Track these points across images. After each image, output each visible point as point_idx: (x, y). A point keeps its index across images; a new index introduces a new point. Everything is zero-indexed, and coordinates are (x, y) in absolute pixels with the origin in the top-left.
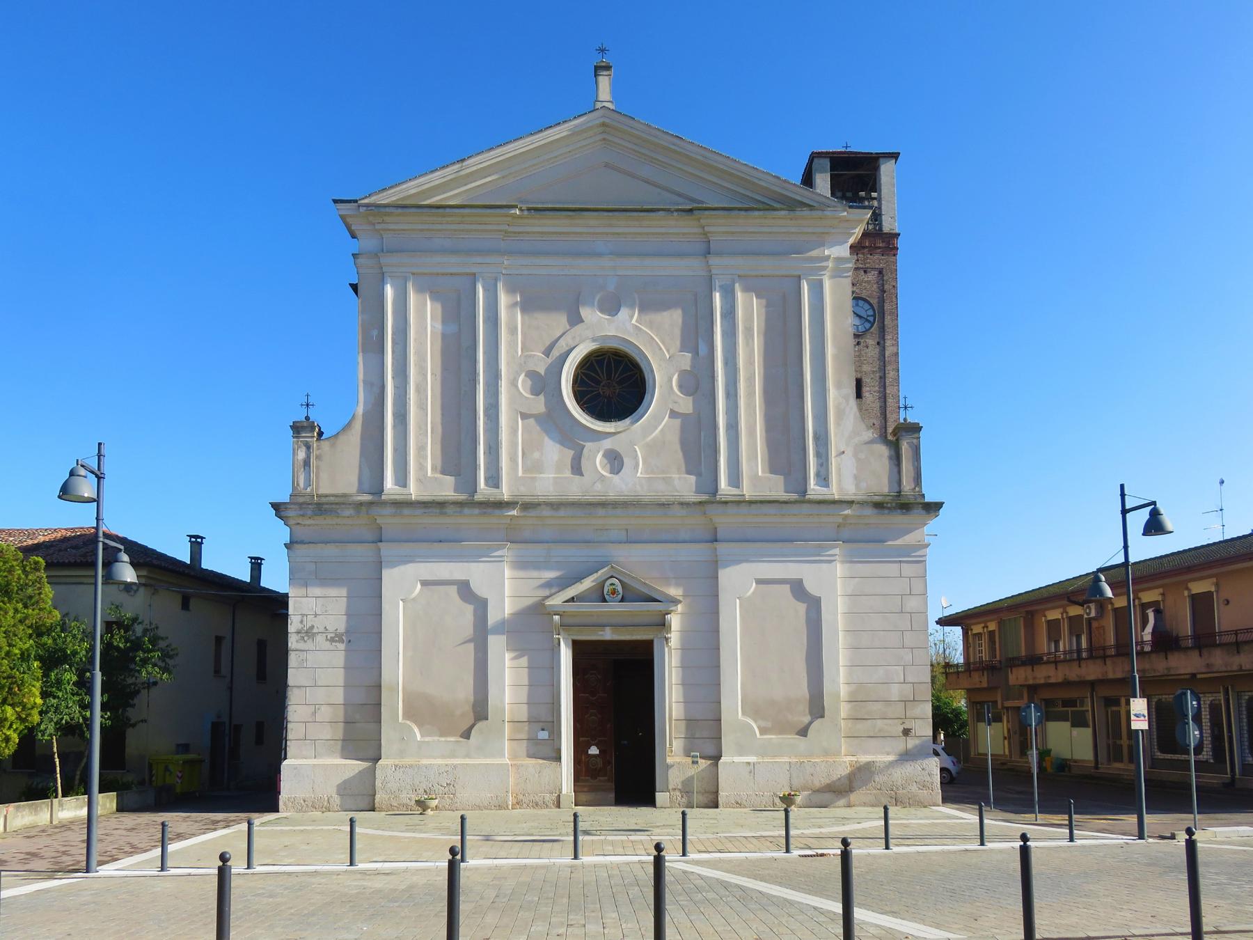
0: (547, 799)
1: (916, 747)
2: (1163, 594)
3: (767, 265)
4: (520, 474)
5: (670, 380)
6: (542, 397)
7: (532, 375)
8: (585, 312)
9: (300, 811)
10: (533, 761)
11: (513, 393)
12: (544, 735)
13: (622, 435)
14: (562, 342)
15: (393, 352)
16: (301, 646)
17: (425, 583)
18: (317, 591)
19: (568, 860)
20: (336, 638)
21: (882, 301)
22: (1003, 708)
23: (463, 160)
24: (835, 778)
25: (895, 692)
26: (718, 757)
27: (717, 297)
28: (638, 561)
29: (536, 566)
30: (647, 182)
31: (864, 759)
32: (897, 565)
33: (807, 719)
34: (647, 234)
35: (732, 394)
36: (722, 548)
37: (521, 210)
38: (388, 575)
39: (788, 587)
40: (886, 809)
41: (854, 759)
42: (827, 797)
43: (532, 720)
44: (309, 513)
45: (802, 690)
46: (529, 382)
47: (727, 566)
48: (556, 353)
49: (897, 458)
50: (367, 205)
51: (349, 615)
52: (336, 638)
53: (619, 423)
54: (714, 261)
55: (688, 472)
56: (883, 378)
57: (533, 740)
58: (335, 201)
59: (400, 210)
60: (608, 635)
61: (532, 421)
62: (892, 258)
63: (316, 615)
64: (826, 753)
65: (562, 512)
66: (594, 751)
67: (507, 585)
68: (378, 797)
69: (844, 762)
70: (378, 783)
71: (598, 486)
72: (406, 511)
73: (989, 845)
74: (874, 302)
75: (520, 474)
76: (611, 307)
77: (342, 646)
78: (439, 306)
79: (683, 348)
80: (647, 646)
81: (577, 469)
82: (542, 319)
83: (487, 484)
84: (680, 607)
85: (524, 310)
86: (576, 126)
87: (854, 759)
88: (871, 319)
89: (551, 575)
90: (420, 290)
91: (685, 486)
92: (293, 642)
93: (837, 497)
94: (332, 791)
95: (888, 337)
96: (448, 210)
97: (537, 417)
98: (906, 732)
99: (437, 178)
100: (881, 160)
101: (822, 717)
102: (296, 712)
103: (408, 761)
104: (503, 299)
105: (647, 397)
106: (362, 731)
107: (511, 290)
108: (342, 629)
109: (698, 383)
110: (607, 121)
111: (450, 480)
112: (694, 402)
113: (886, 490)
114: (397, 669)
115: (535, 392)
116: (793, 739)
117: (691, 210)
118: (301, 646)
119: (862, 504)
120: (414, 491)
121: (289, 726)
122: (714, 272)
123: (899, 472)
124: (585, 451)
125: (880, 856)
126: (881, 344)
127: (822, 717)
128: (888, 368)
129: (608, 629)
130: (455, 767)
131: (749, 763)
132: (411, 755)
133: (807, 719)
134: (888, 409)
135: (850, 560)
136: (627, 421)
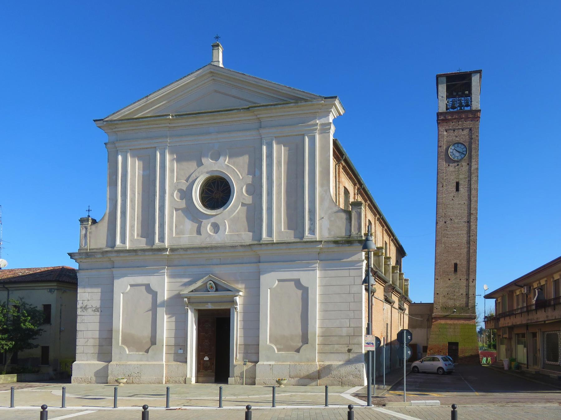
0: (180, 380)
1: (354, 358)
2: (546, 281)
4: (174, 236)
5: (242, 189)
6: (184, 201)
7: (180, 191)
8: (204, 160)
9: (80, 383)
10: (176, 363)
11: (171, 199)
12: (181, 351)
13: (219, 216)
14: (194, 175)
15: (121, 185)
16: (82, 313)
17: (132, 286)
18: (89, 290)
19: (111, 408)
20: (96, 310)
21: (470, 143)
23: (147, 96)
24: (311, 372)
25: (344, 332)
26: (257, 362)
27: (264, 148)
28: (223, 273)
29: (180, 276)
30: (234, 97)
31: (327, 363)
33: (300, 344)
34: (232, 121)
35: (270, 194)
36: (262, 265)
37: (172, 116)
38: (117, 282)
39: (293, 283)
40: (326, 387)
41: (323, 363)
42: (307, 380)
43: (176, 345)
44: (84, 257)
45: (299, 331)
46: (179, 194)
47: (265, 274)
48: (191, 180)
49: (349, 219)
50: (107, 121)
51: (102, 300)
52: (96, 310)
53: (218, 210)
54: (262, 131)
55: (249, 231)
56: (470, 181)
57: (176, 354)
58: (95, 121)
59: (120, 122)
60: (210, 307)
61: (180, 211)
63: (88, 300)
64: (308, 360)
65: (189, 252)
66: (206, 358)
67: (166, 286)
68: (109, 377)
69: (318, 364)
70: (109, 372)
71: (208, 240)
72: (122, 254)
73: (278, 407)
74: (467, 144)
75: (174, 236)
76: (216, 158)
77: (98, 313)
78: (141, 163)
79: (249, 174)
80: (229, 310)
81: (199, 232)
82: (185, 164)
83: (159, 240)
84: (241, 293)
85: (177, 162)
86: (198, 75)
87: (323, 363)
89: (186, 280)
90: (133, 156)
91: (247, 237)
92: (79, 312)
93: (318, 239)
94: (92, 375)
95: (473, 161)
96: (140, 120)
97: (183, 210)
98: (349, 351)
99: (137, 106)
101: (307, 343)
102: (80, 341)
103: (123, 362)
104: (168, 157)
105: (231, 197)
106: (105, 351)
107: (171, 153)
108: (98, 306)
109: (254, 189)
110: (212, 70)
111: (144, 240)
112: (253, 198)
113: (344, 235)
114: (120, 323)
115: (181, 198)
116: (293, 353)
117: (248, 108)
118: (82, 313)
119: (327, 242)
120: (128, 246)
121: (77, 347)
122: (263, 136)
123: (351, 226)
124: (203, 224)
125: (8, 411)
126: (469, 164)
127: (307, 343)
128: (473, 176)
129: (209, 304)
130: (141, 365)
131: (270, 365)
132: (125, 359)
133: (300, 344)
135: (324, 269)
136: (222, 209)
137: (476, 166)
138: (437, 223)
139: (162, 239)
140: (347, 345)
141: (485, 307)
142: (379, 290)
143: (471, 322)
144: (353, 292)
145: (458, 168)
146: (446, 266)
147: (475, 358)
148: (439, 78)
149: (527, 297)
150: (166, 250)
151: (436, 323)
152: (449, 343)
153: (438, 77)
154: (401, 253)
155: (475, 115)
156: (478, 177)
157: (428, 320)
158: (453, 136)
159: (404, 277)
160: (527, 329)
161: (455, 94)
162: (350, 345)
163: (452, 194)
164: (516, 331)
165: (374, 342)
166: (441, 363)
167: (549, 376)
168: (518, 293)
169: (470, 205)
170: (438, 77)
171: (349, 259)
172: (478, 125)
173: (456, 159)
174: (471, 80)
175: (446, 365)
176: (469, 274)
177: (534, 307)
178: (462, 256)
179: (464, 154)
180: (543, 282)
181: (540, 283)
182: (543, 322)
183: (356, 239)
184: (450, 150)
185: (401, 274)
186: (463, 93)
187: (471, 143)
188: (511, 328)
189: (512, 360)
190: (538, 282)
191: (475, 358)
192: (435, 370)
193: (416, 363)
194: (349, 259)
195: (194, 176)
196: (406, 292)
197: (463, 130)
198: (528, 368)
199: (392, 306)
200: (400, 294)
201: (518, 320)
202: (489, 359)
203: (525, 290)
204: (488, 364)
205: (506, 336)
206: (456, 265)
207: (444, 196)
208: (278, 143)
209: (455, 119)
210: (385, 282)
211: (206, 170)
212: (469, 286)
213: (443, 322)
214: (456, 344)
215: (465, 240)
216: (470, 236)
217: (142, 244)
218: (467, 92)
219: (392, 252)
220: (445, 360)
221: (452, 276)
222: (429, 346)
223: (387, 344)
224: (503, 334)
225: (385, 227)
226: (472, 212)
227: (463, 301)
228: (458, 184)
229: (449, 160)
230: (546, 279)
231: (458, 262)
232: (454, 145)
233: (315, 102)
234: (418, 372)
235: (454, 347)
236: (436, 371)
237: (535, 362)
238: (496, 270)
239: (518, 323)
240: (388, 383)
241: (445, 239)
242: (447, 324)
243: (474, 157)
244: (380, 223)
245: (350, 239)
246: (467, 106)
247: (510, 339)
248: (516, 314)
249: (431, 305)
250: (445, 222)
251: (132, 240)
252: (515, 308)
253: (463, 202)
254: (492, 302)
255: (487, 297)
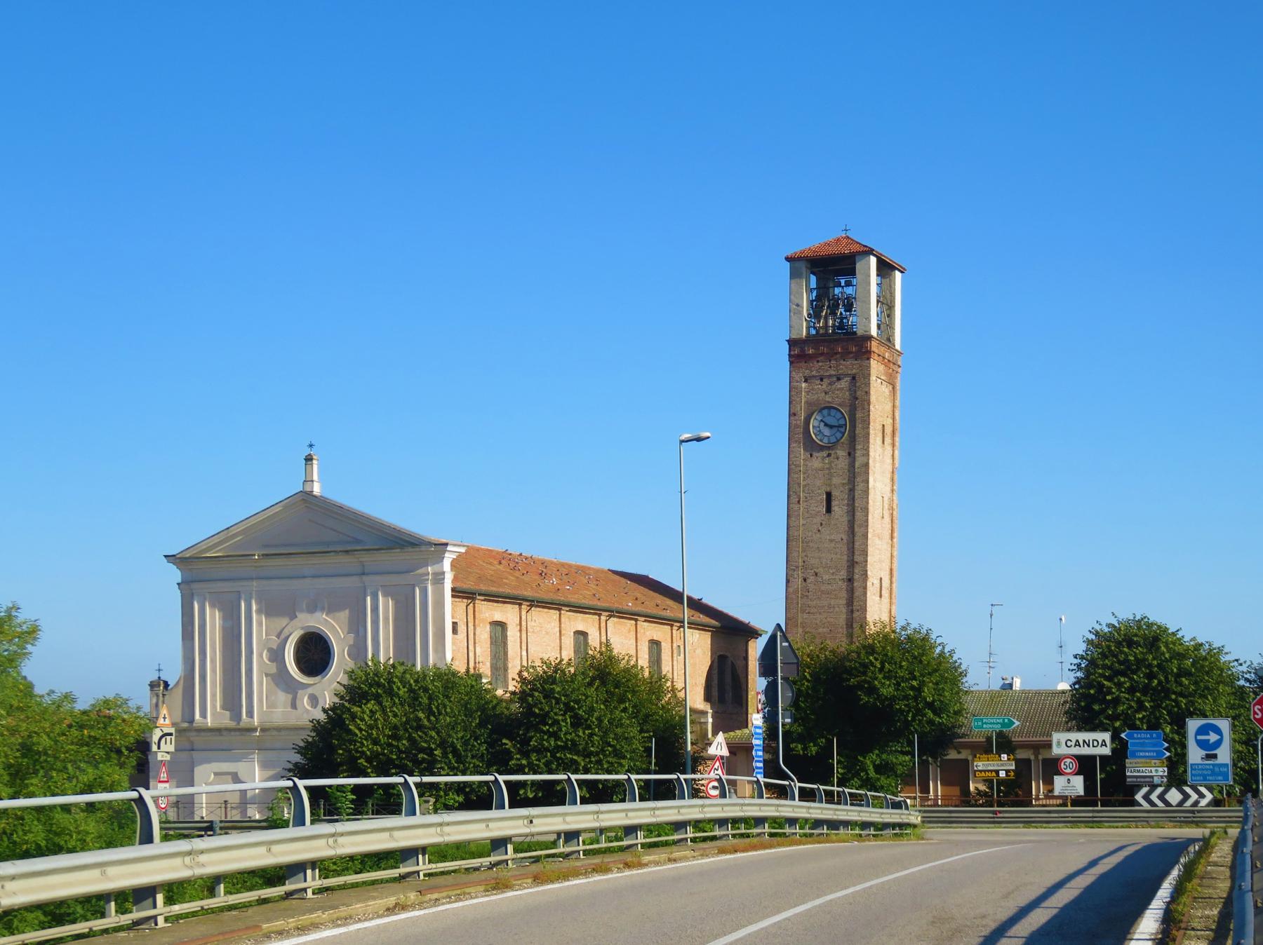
3: (394, 579)
7: (270, 650)
11: (259, 661)
48: (283, 636)
56: (852, 490)
65: (283, 733)
76: (312, 609)
81: (294, 706)
90: (213, 606)
95: (858, 447)
120: (209, 722)
128: (858, 479)
134: (857, 523)
138: (788, 581)
139: (250, 714)
145: (830, 463)
150: (255, 730)
163: (818, 520)
195: (286, 632)
208: (385, 595)
209: (822, 354)
211: (300, 625)
216: (852, 611)
217: (226, 721)
226: (857, 558)
229: (811, 446)
232: (820, 411)
233: (423, 548)
241: (805, 616)
243: (859, 439)
251: (214, 714)
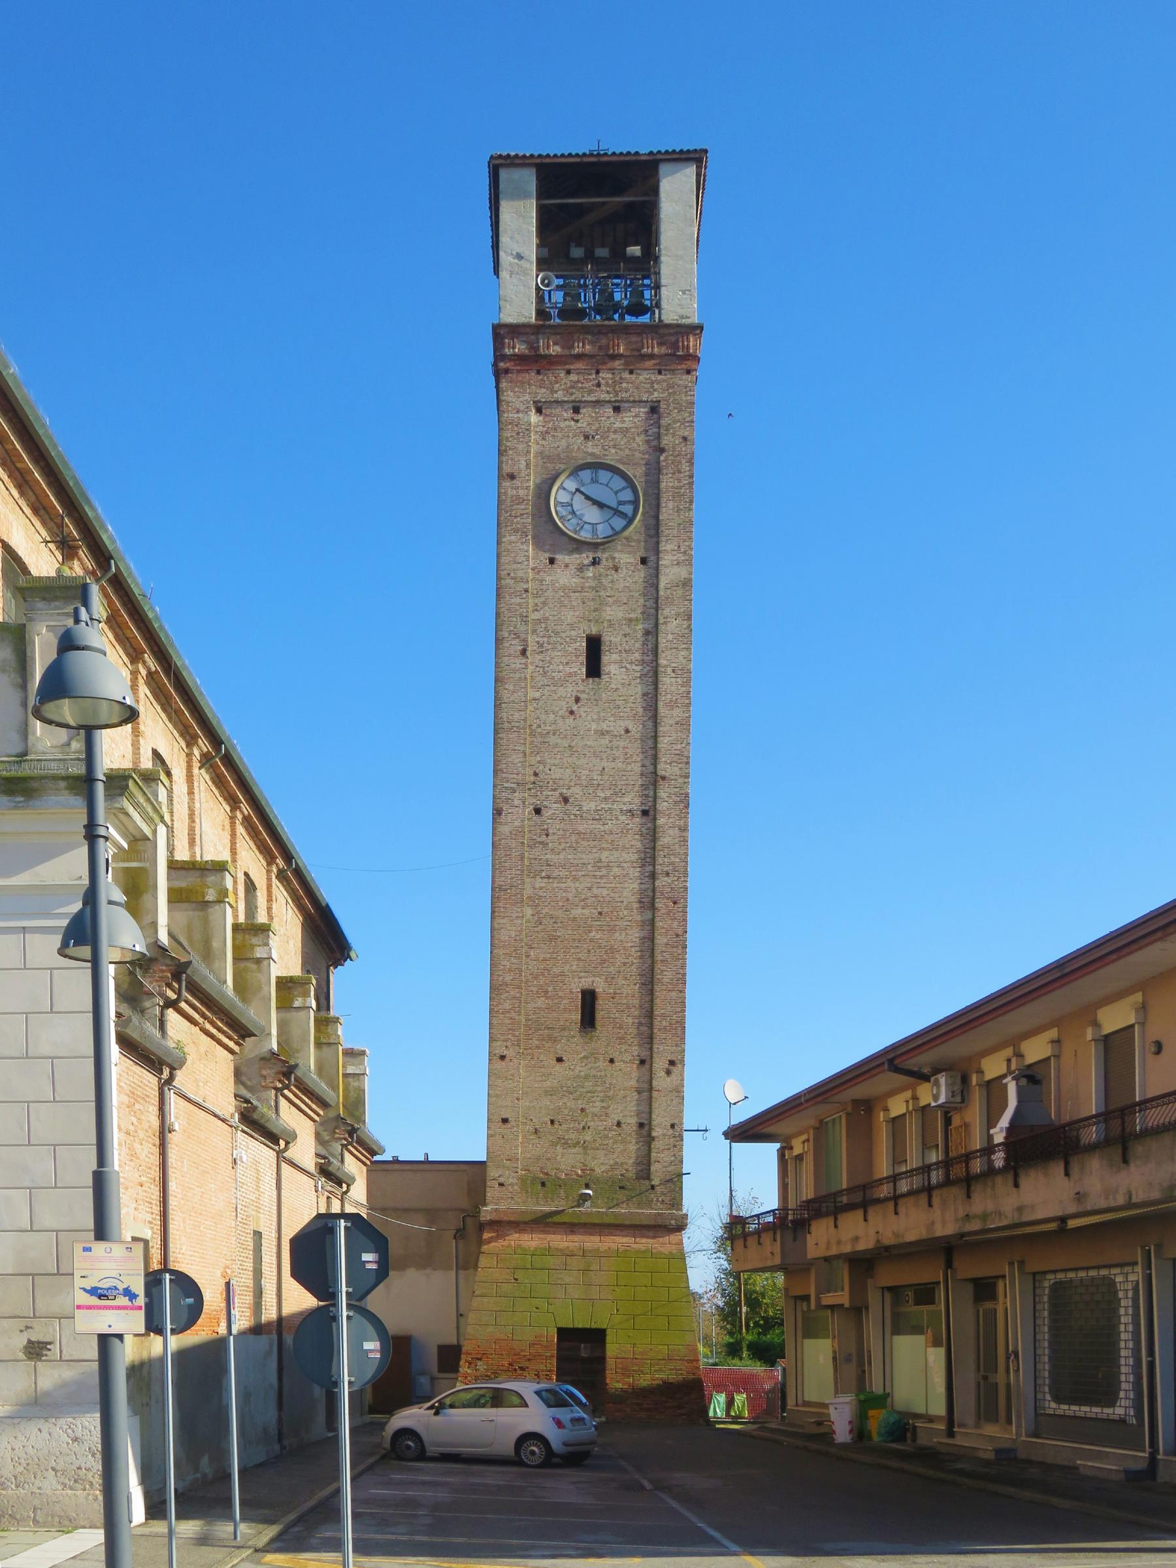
1: (64, 1385)
2: (1056, 1042)
21: (654, 472)
22: (821, 1307)
32: (14, 939)
56: (652, 633)
62: (683, 380)
74: (637, 473)
88: (628, 509)
95: (666, 546)
98: (36, 1350)
100: (663, 169)
126: (649, 561)
128: (666, 611)
134: (663, 700)
137: (683, 572)
138: (497, 812)
140: (21, 1323)
141: (727, 1183)
142: (208, 1069)
143: (662, 1244)
144: (46, 1050)
145: (598, 577)
146: (541, 1002)
147: (684, 1396)
148: (504, 174)
149: (948, 1121)
151: (498, 1250)
152: (562, 1332)
153: (497, 165)
154: (327, 940)
155: (675, 346)
156: (689, 618)
157: (460, 1234)
158: (569, 436)
159: (346, 1036)
160: (949, 1265)
161: (577, 252)
162: (35, 1323)
163: (570, 690)
164: (888, 1276)
165: (139, 1287)
166: (534, 1417)
167: (1076, 1468)
168: (898, 1106)
169: (655, 737)
170: (497, 165)
171: (23, 879)
172: (688, 390)
173: (585, 535)
174: (655, 190)
175: (559, 1423)
176: (651, 1038)
177: (999, 1159)
178: (620, 959)
179: (623, 515)
180: (1036, 1050)
181: (1019, 1055)
182: (1053, 1226)
183: (55, 769)
184: (558, 496)
185: (325, 1022)
186: (618, 254)
187: (659, 470)
188: (863, 1264)
189: (869, 1402)
190: (1009, 1052)
191: (684, 1396)
192: (507, 1447)
193: (410, 1417)
194: (23, 879)
196: (356, 1104)
197: (617, 409)
198: (951, 1434)
199: (280, 1154)
200: (324, 1104)
201: (912, 1224)
202: (740, 1399)
203: (936, 1093)
204: (736, 1420)
205: (842, 1297)
206: (589, 999)
207: (532, 694)
210: (241, 1031)
212: (651, 1089)
213: (531, 1241)
214: (597, 1336)
215: (630, 889)
216: (653, 876)
218: (635, 250)
219: (286, 951)
220: (553, 1400)
221: (574, 1044)
222: (467, 1347)
223: (257, 1329)
224: (818, 1294)
225: (246, 808)
226: (663, 768)
227: (627, 1153)
228: (594, 647)
229: (552, 537)
230: (1053, 1033)
231: (600, 986)
232: (575, 472)
234: (422, 1455)
235: (584, 1351)
236: (508, 1449)
237: (990, 1405)
238: (780, 1010)
239: (911, 1237)
240: (255, 1509)
241: (539, 883)
242: (549, 1251)
244: (219, 781)
245: (25, 771)
246: (638, 309)
247: (857, 1310)
248: (896, 1198)
249: (471, 1176)
250: (538, 811)
252: (883, 1168)
253: (623, 724)
254: (763, 1157)
255: (744, 1132)
